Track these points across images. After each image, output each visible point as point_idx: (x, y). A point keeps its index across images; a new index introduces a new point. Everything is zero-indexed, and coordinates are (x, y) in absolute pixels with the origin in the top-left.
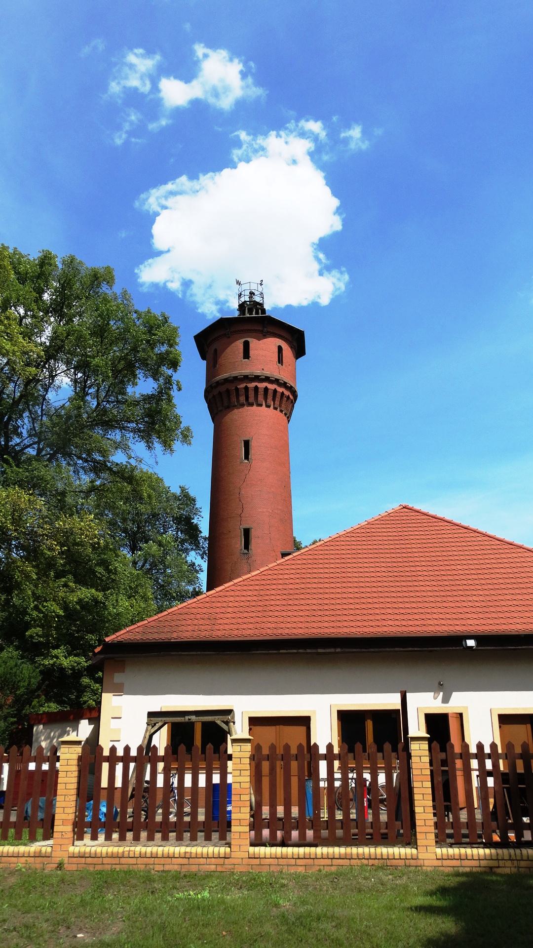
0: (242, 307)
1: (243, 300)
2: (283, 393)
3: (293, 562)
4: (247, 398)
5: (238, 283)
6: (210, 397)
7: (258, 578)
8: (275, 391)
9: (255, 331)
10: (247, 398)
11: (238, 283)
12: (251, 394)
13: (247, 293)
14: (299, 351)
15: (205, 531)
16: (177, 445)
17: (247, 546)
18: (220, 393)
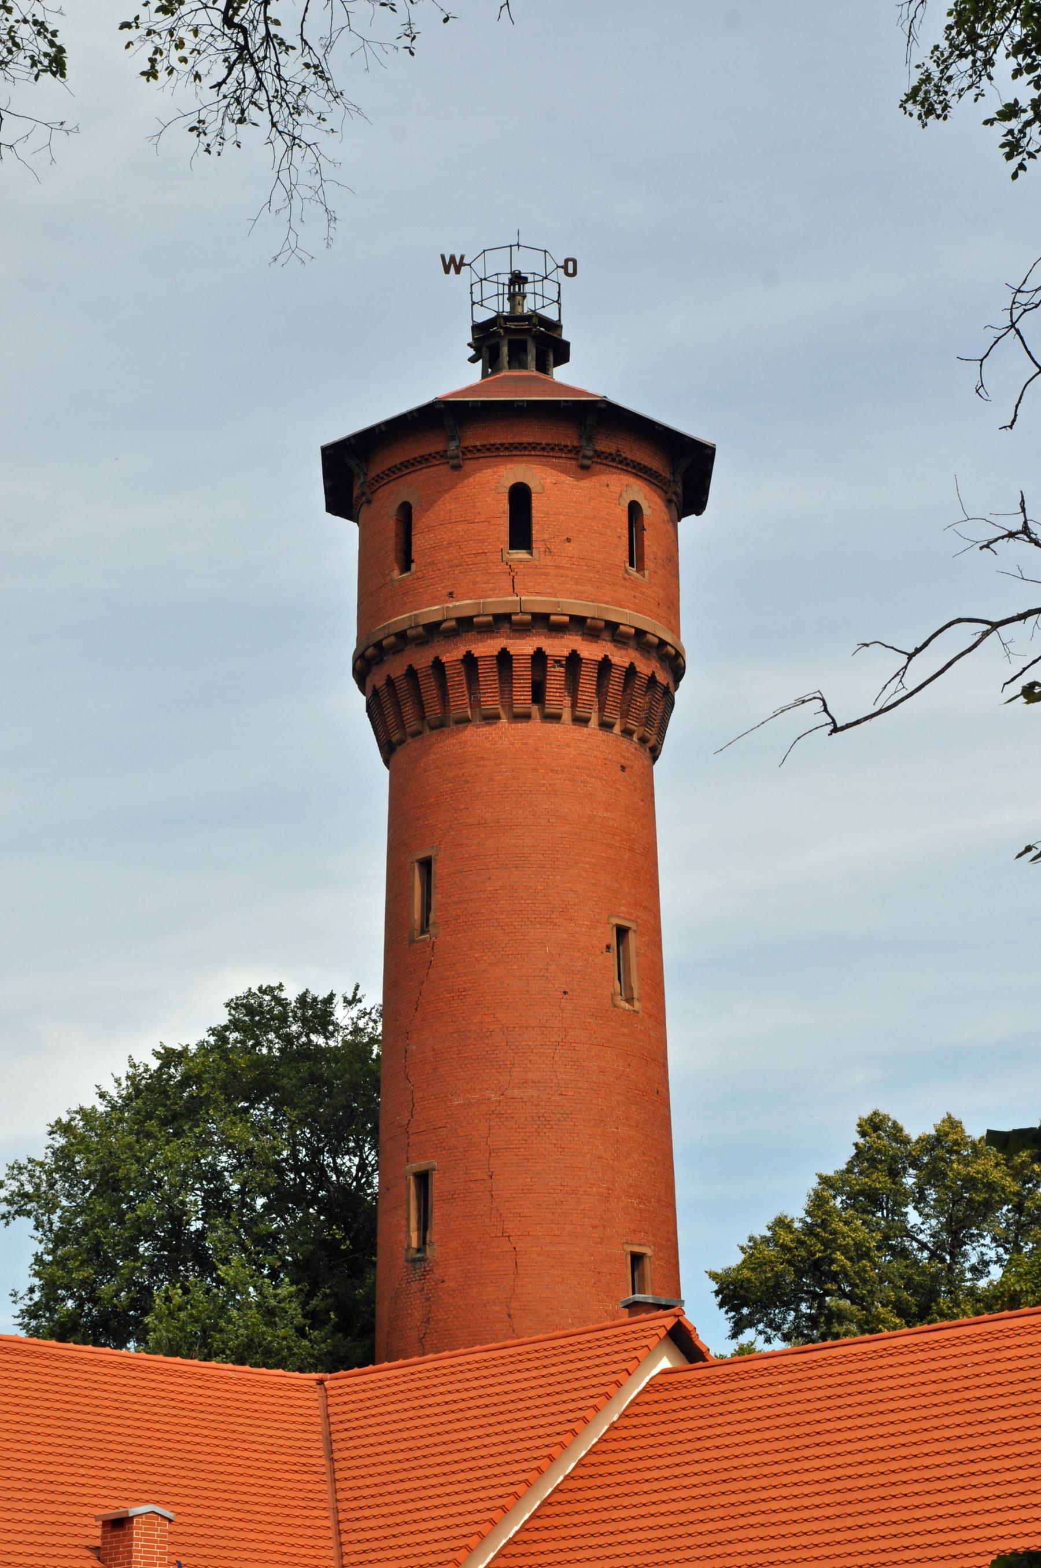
9: (425, 460)
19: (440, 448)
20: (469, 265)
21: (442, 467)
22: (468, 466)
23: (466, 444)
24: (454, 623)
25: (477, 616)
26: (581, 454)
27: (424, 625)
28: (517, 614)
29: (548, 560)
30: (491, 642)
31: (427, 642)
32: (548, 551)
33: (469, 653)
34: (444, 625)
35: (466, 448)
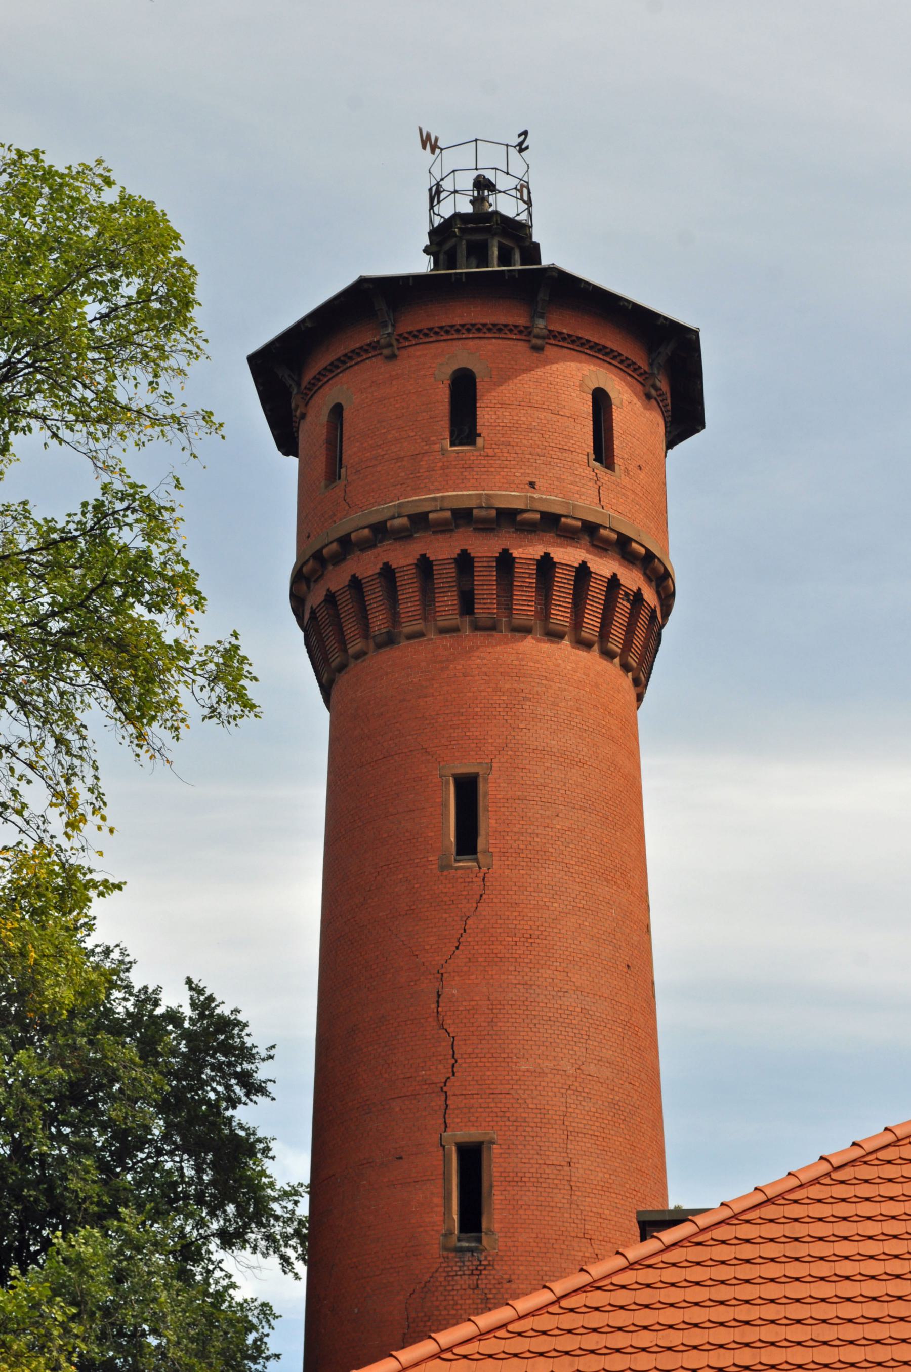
0: (442, 239)
1: (446, 209)
2: (614, 582)
3: (696, 1254)
4: (467, 604)
5: (429, 143)
6: (316, 598)
7: (544, 1322)
8: (583, 572)
9: (498, 329)
10: (467, 604)
11: (429, 143)
12: (486, 584)
13: (466, 182)
14: (684, 417)
15: (289, 1165)
16: (241, 1017)
17: (472, 1218)
18: (356, 584)
19: (522, 321)
20: (442, 150)
21: (520, 343)
22: (550, 351)
23: (551, 327)
24: (538, 516)
25: (566, 517)
26: (650, 382)
27: (497, 509)
28: (605, 527)
29: (625, 481)
30: (570, 550)
31: (492, 530)
32: (627, 471)
33: (547, 555)
34: (526, 516)
35: (400, 335)
